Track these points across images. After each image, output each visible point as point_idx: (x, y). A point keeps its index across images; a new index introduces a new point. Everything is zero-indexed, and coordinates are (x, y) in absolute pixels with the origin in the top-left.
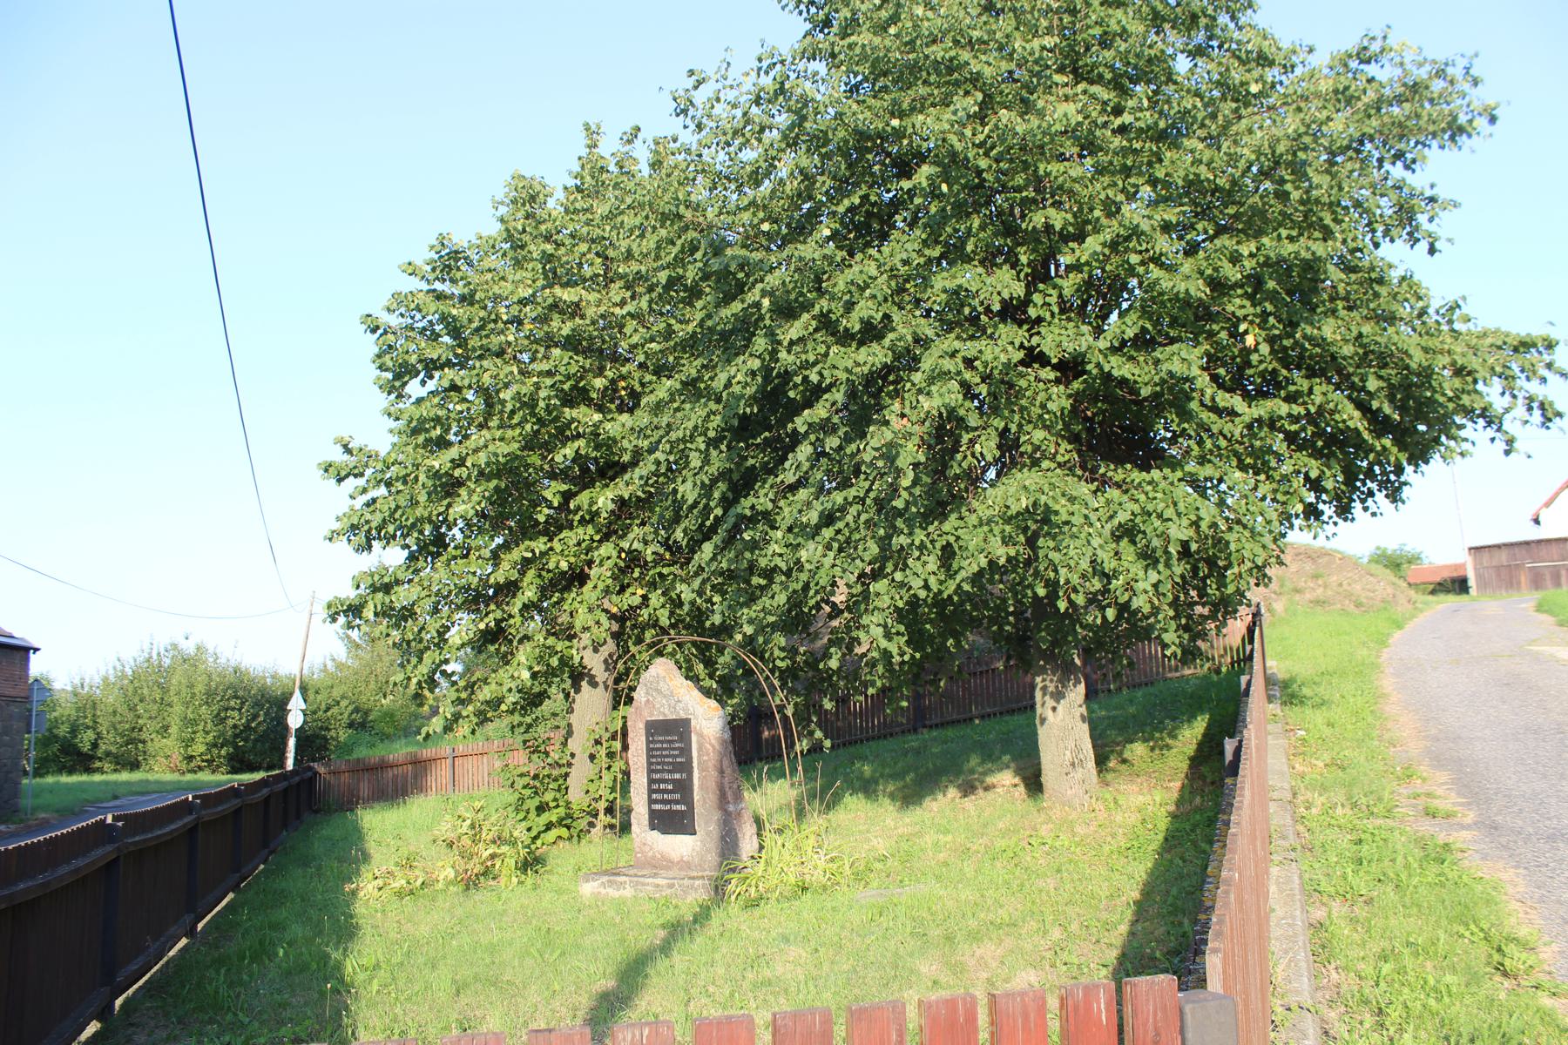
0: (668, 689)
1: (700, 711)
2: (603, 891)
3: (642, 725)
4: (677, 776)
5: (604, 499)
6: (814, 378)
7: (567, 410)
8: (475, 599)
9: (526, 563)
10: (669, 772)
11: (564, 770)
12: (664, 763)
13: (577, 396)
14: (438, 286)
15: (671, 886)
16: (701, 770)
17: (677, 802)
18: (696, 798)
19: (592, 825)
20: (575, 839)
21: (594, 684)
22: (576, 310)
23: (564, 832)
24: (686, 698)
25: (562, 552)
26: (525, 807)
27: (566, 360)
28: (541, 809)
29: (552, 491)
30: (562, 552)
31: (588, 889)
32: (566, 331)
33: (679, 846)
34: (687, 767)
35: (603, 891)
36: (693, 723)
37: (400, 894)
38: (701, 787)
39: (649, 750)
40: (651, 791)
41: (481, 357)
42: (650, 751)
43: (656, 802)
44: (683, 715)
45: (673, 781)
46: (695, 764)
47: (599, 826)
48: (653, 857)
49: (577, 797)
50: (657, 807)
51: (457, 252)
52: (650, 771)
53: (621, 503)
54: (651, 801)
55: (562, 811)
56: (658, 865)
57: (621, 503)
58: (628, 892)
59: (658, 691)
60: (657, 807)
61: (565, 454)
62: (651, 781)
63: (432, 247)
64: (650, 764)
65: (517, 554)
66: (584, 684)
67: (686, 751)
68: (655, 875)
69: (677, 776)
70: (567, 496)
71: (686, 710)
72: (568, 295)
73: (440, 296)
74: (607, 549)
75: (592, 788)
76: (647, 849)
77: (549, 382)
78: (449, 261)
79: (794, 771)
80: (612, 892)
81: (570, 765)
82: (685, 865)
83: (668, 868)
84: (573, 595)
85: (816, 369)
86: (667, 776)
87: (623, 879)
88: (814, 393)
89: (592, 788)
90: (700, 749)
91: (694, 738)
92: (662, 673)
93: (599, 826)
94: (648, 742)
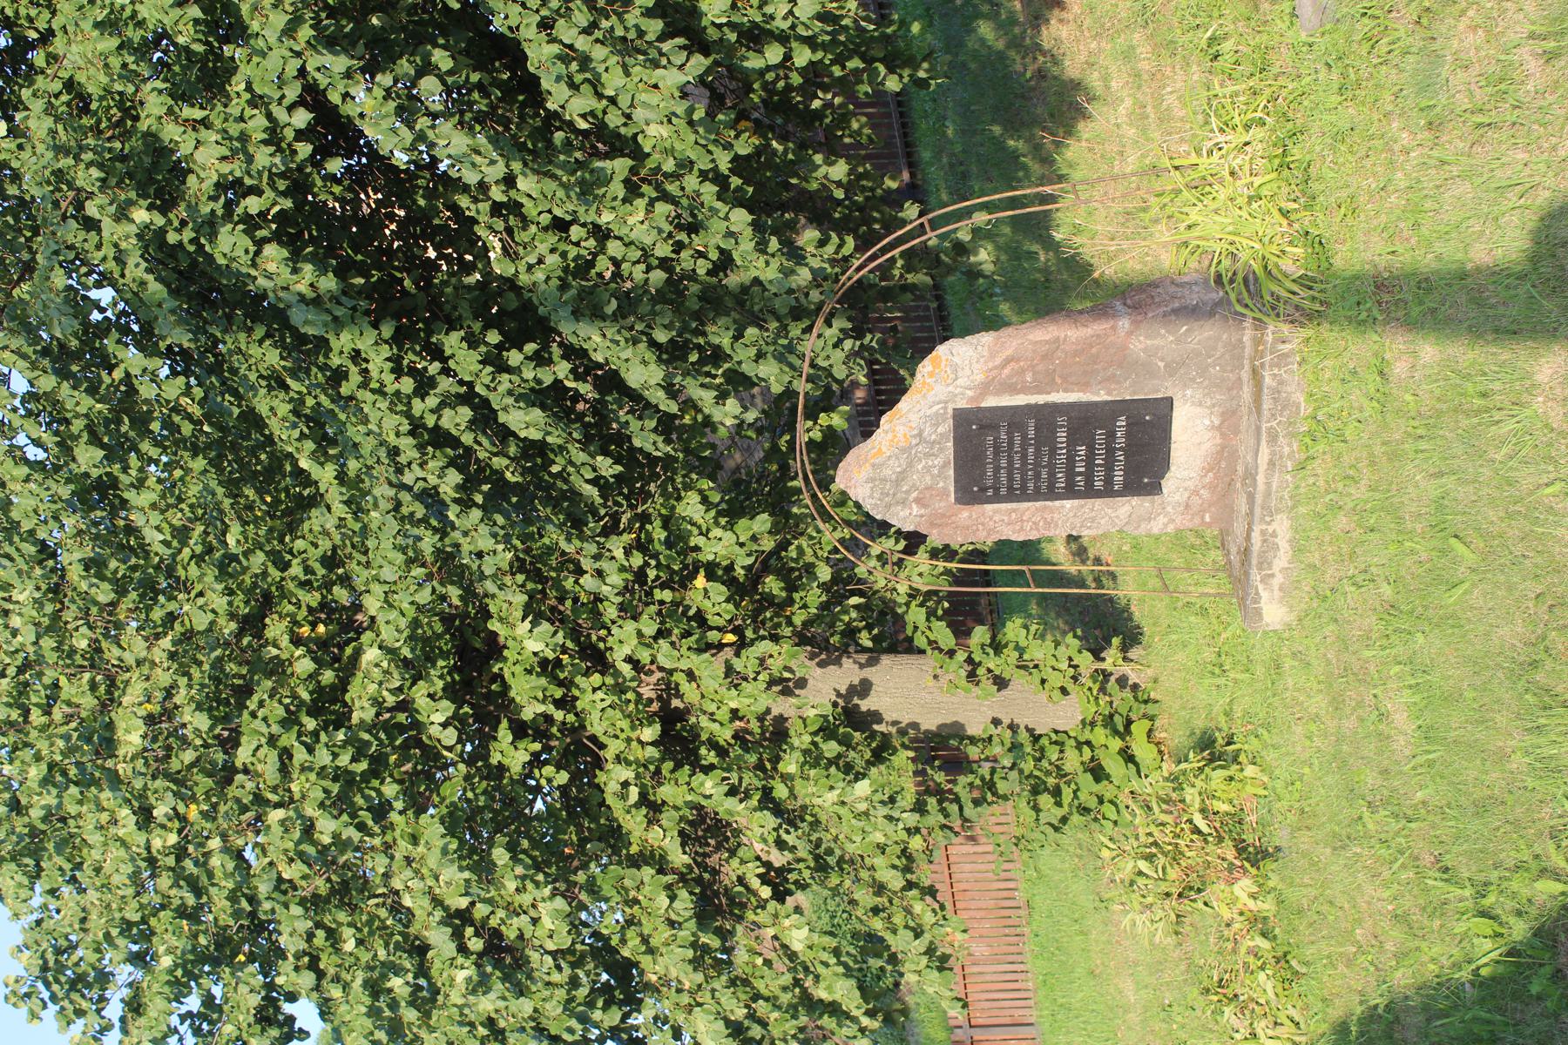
0: (899, 468)
1: (940, 391)
2: (1278, 580)
3: (966, 514)
4: (1062, 436)
5: (529, 641)
6: (302, 118)
7: (356, 717)
8: (716, 906)
9: (652, 807)
10: (1053, 452)
11: (1023, 736)
12: (1037, 464)
13: (329, 705)
14: (114, 1010)
15: (1273, 438)
16: (1051, 387)
17: (1111, 435)
18: (1102, 396)
19: (1122, 681)
20: (1151, 709)
21: (864, 688)
22: (160, 720)
23: (1140, 729)
24: (915, 419)
25: (622, 739)
26: (1092, 803)
27: (258, 724)
28: (1098, 773)
29: (511, 754)
30: (622, 739)
31: (1273, 612)
32: (202, 722)
33: (1191, 435)
34: (1045, 416)
35: (1278, 580)
36: (962, 404)
37: (1289, 979)
38: (1084, 386)
39: (1011, 496)
40: (1090, 492)
41: (252, 900)
42: (1016, 494)
43: (1109, 481)
44: (947, 427)
45: (1072, 443)
46: (1040, 399)
47: (1126, 669)
48: (1212, 487)
49: (1068, 714)
50: (1119, 476)
51: (45, 968)
52: (1052, 494)
53: (533, 612)
54: (1108, 492)
55: (1100, 735)
56: (1227, 472)
57: (533, 612)
58: (1282, 527)
59: (901, 477)
60: (1119, 476)
61: (436, 716)
62: (1071, 492)
63: (34, 1016)
64: (1037, 496)
65: (633, 823)
66: (865, 705)
67: (1015, 418)
68: (1250, 475)
69: (1062, 436)
70: (520, 731)
71: (936, 420)
72: (131, 736)
73: (135, 1006)
74: (623, 642)
75: (1056, 680)
76: (1196, 500)
77: (300, 755)
78: (64, 979)
79: (1052, 199)
80: (1281, 561)
81: (1013, 727)
82: (1228, 424)
83: (1233, 456)
84: (704, 722)
85: (280, 114)
86: (1062, 457)
87: (1256, 537)
88: (333, 130)
89: (1056, 680)
90: (1013, 390)
91: (991, 402)
92: (865, 472)
93: (1126, 669)
94: (997, 498)
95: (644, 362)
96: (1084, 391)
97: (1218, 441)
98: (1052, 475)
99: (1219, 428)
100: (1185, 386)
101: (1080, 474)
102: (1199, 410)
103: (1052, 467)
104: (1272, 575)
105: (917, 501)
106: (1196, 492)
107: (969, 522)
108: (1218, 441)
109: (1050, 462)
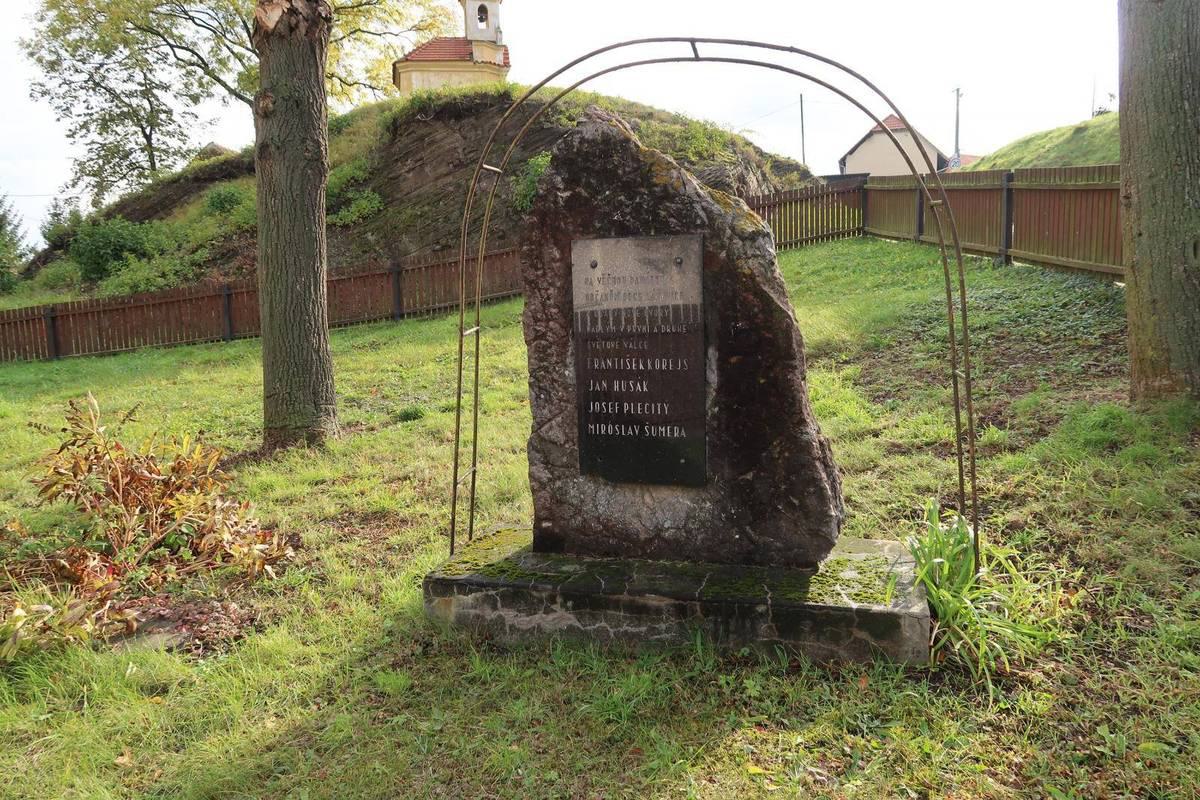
10: (642, 355)
17: (665, 421)
35: (490, 615)
43: (599, 418)
48: (583, 529)
69: (661, 364)
95: (191, 353)
96: (719, 391)
97: (643, 536)
98: (606, 355)
99: (284, 446)
100: (716, 502)
101: (611, 386)
102: (683, 515)
103: (620, 354)
104: (495, 608)
105: (575, 197)
106: (578, 511)
107: (547, 258)
108: (643, 536)
109: (628, 351)
